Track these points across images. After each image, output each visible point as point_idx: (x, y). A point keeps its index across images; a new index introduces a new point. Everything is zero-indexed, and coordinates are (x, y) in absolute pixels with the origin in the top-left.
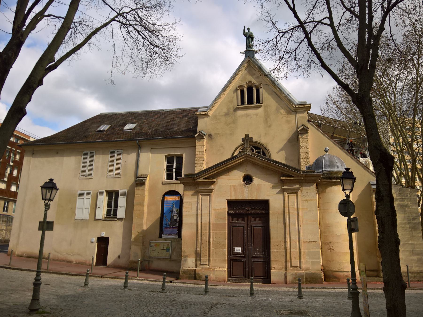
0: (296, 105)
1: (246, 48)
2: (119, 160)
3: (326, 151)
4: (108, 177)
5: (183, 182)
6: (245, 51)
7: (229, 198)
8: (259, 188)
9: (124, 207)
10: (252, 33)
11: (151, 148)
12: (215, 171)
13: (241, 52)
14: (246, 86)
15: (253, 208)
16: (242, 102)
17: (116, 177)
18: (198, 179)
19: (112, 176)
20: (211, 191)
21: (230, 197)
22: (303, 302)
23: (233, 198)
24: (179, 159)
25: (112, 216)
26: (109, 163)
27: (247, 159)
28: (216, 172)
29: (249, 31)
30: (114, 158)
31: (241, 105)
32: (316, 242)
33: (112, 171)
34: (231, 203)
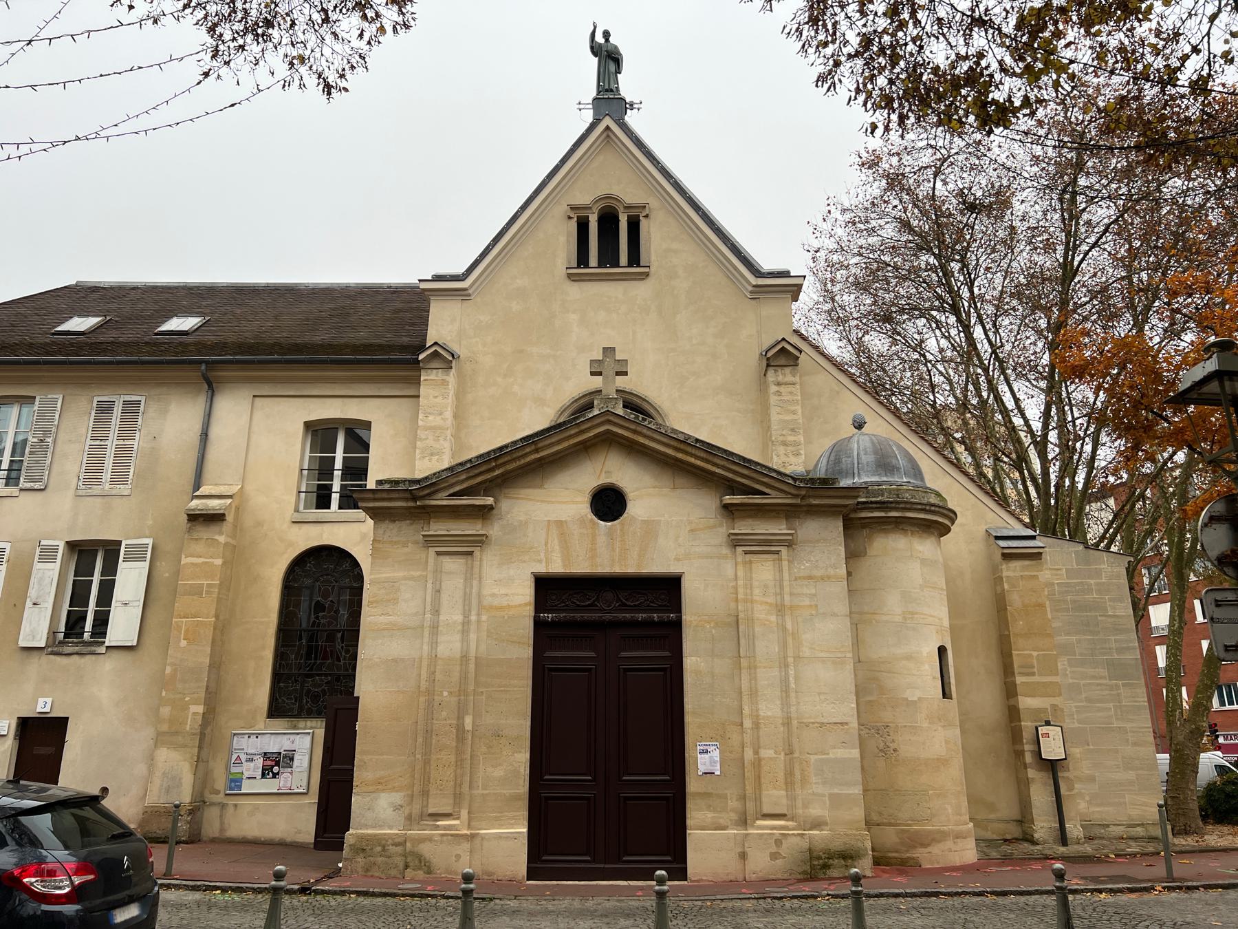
0: (757, 273)
1: (599, 92)
2: (127, 431)
4: (80, 493)
5: (371, 505)
6: (595, 99)
7: (542, 569)
8: (650, 529)
9: (136, 604)
10: (616, 47)
11: (254, 396)
12: (492, 470)
13: (580, 103)
14: (596, 209)
15: (626, 605)
16: (583, 260)
18: (428, 495)
19: (97, 490)
20: (480, 541)
21: (544, 564)
22: (399, 849)
23: (557, 567)
24: (357, 436)
25: (86, 636)
26: (89, 442)
27: (608, 431)
28: (497, 472)
29: (607, 40)
30: (107, 423)
31: (579, 267)
34: (546, 586)
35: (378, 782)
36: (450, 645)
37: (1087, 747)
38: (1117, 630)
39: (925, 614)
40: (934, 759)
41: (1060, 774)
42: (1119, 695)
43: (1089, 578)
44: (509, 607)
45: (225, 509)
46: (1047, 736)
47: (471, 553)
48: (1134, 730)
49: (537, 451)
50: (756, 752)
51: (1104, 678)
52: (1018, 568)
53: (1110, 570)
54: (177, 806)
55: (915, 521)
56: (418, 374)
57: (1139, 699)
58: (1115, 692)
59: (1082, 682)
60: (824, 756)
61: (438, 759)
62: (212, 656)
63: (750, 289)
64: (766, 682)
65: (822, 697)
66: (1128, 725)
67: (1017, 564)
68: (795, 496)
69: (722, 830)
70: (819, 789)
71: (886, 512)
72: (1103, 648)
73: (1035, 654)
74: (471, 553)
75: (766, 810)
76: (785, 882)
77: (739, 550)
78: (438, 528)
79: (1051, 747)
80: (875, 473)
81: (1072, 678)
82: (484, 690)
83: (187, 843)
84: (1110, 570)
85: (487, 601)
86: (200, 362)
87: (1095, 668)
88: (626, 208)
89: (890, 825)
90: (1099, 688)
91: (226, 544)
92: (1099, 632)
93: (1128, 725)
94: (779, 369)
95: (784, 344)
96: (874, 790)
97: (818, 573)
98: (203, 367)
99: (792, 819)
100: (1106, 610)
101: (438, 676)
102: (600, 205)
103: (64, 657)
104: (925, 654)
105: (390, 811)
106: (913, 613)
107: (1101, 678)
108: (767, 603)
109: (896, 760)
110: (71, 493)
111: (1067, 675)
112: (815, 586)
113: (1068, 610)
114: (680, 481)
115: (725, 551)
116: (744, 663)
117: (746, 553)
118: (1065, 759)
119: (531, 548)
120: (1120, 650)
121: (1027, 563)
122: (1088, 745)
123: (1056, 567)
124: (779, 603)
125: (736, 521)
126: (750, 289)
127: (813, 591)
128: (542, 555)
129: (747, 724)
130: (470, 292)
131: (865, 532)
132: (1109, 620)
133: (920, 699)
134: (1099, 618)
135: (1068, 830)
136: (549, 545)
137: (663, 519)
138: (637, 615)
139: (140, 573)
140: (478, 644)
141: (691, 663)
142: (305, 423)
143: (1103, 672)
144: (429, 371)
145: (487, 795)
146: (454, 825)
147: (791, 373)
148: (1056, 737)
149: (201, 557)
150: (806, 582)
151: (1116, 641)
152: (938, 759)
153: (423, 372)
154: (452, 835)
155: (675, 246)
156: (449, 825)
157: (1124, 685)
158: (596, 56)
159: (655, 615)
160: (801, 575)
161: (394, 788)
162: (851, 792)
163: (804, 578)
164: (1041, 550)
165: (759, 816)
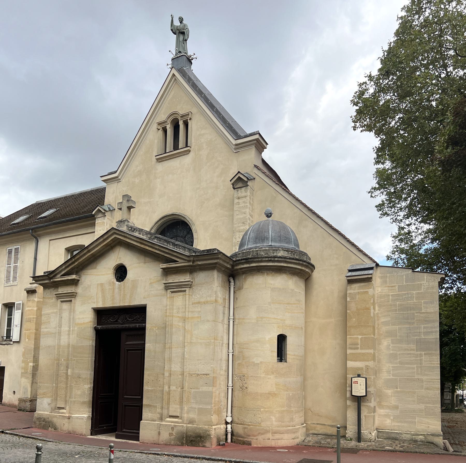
3: (269, 215)
4: (6, 285)
11: (50, 240)
13: (168, 65)
14: (169, 122)
17: (13, 284)
20: (73, 295)
21: (96, 304)
32: (208, 374)
33: (9, 276)
35: (44, 394)
36: (64, 340)
37: (396, 390)
38: (426, 321)
39: (270, 318)
40: (266, 393)
41: (362, 404)
42: (421, 360)
43: (412, 290)
44: (84, 323)
45: (35, 288)
46: (356, 382)
47: (71, 301)
48: (427, 380)
49: (292, 242)
50: (169, 388)
51: (414, 350)
52: (357, 288)
53: (427, 284)
54: (19, 400)
55: (268, 268)
56: (93, 221)
57: (434, 362)
58: (419, 358)
59: (398, 353)
60: (197, 390)
61: (60, 386)
62: (35, 345)
63: (234, 147)
64: (175, 355)
65: (199, 362)
66: (424, 378)
67: (356, 286)
68: (189, 261)
69: (154, 421)
70: (194, 406)
71: (249, 264)
72: (415, 333)
73: (360, 337)
74: (71, 301)
75: (171, 414)
76: (167, 445)
77: (169, 291)
78: (62, 290)
79: (358, 389)
80: (255, 242)
81: (392, 350)
82: (75, 359)
83: (30, 412)
84: (427, 284)
85: (77, 321)
86: (29, 230)
87: (408, 344)
88: (182, 117)
89: (241, 424)
90: (409, 355)
91: (38, 302)
92: (414, 323)
93: (424, 378)
94: (239, 189)
95: (239, 175)
96: (237, 407)
97: (202, 300)
98: (31, 231)
99: (181, 419)
100: (421, 309)
101: (61, 353)
102: (171, 118)
103: (3, 345)
104: (267, 339)
105: (47, 405)
106: (262, 318)
107: (411, 350)
108: (178, 317)
109: (246, 393)
110: (3, 286)
111: (390, 348)
112: (201, 307)
113: (396, 310)
114: (147, 259)
115: (164, 292)
116: (167, 346)
117: (172, 292)
118: (366, 396)
119: (92, 297)
120: (426, 333)
121: (362, 284)
122: (397, 388)
123: (392, 285)
124: (184, 316)
125: (168, 276)
126: (234, 147)
127: (200, 310)
128: (95, 300)
129: (167, 374)
130: (119, 178)
131: (244, 276)
132: (422, 315)
133: (261, 362)
134: (416, 314)
135: (362, 434)
136: (98, 295)
137: (140, 279)
138: (130, 325)
139: (20, 314)
140: (73, 339)
141: (148, 346)
142: (65, 249)
143: (413, 346)
144: (98, 218)
145: (75, 401)
146: (64, 412)
147: (245, 191)
148: (362, 384)
149: (30, 307)
150: (197, 305)
151: (424, 328)
152: (268, 393)
153: (96, 220)
154: (62, 416)
155: (203, 132)
156: (63, 412)
157: (425, 354)
158: (175, 34)
159: (137, 325)
160: (195, 301)
161: (48, 396)
162: (207, 407)
163: (196, 303)
164: (370, 276)
165: (168, 416)
